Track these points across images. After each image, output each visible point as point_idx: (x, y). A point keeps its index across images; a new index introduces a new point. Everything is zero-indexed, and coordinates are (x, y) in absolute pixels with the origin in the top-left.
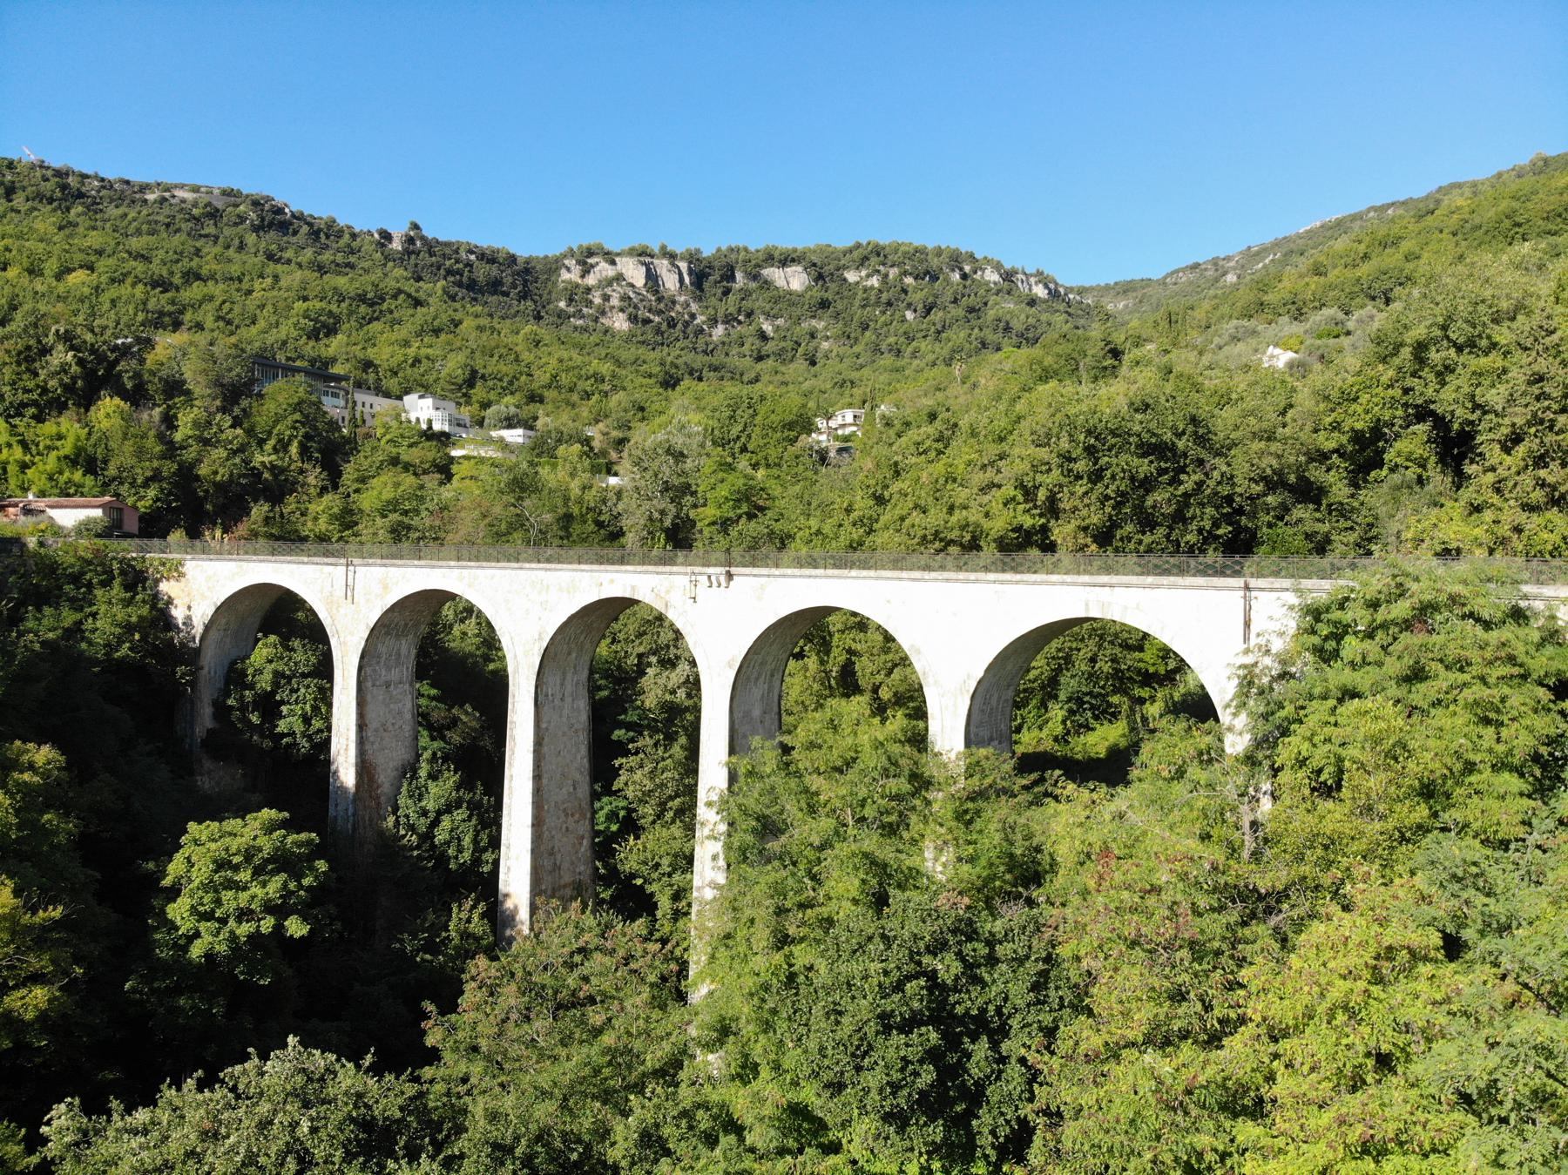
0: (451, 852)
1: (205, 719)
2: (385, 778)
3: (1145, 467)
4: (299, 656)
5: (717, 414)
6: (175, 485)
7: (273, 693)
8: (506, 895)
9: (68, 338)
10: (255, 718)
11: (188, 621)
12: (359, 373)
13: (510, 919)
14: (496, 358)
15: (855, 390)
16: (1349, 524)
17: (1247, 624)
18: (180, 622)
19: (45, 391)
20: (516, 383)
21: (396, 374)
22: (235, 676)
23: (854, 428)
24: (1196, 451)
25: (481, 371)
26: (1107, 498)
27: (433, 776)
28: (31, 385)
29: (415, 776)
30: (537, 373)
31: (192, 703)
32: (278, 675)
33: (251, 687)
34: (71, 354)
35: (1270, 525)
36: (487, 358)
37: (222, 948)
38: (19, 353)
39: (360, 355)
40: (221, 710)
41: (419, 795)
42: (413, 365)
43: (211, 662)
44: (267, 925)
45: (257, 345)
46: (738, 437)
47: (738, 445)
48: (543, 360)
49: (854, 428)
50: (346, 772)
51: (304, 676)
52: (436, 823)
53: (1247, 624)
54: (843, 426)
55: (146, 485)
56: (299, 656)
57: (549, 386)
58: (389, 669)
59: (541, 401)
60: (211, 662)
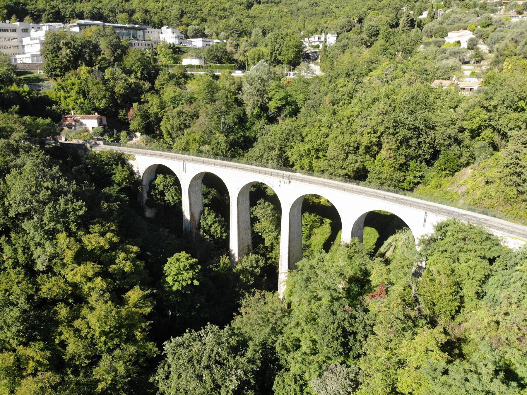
0: (215, 234)
1: (146, 197)
2: (197, 216)
3: (409, 134)
4: (169, 180)
5: (270, 40)
6: (111, 99)
7: (163, 190)
8: (232, 250)
9: (67, 44)
10: (159, 197)
11: (138, 172)
12: (144, 15)
13: (233, 256)
14: (189, 4)
15: (317, 8)
16: (468, 150)
17: (425, 221)
18: (136, 172)
19: (62, 63)
20: (197, 15)
21: (156, 14)
22: (152, 186)
23: (318, 43)
24: (425, 129)
25: (185, 11)
26: (398, 140)
27: (209, 214)
28: (58, 61)
29: (204, 215)
30: (204, 10)
31: (142, 193)
32: (164, 186)
33: (157, 189)
34: (68, 50)
35: (445, 150)
36: (186, 4)
37: (180, 288)
38: (52, 50)
39: (144, 8)
40: (149, 193)
41: (205, 219)
42: (161, 10)
43: (145, 182)
44: (189, 282)
45: (109, 6)
46: (278, 49)
47: (278, 52)
48: (206, 4)
49: (318, 43)
50: (187, 215)
51: (171, 185)
52: (211, 227)
53: (425, 221)
54: (315, 42)
55: (102, 99)
56: (169, 180)
57: (208, 15)
58: (195, 187)
59: (206, 21)
60: (145, 182)
